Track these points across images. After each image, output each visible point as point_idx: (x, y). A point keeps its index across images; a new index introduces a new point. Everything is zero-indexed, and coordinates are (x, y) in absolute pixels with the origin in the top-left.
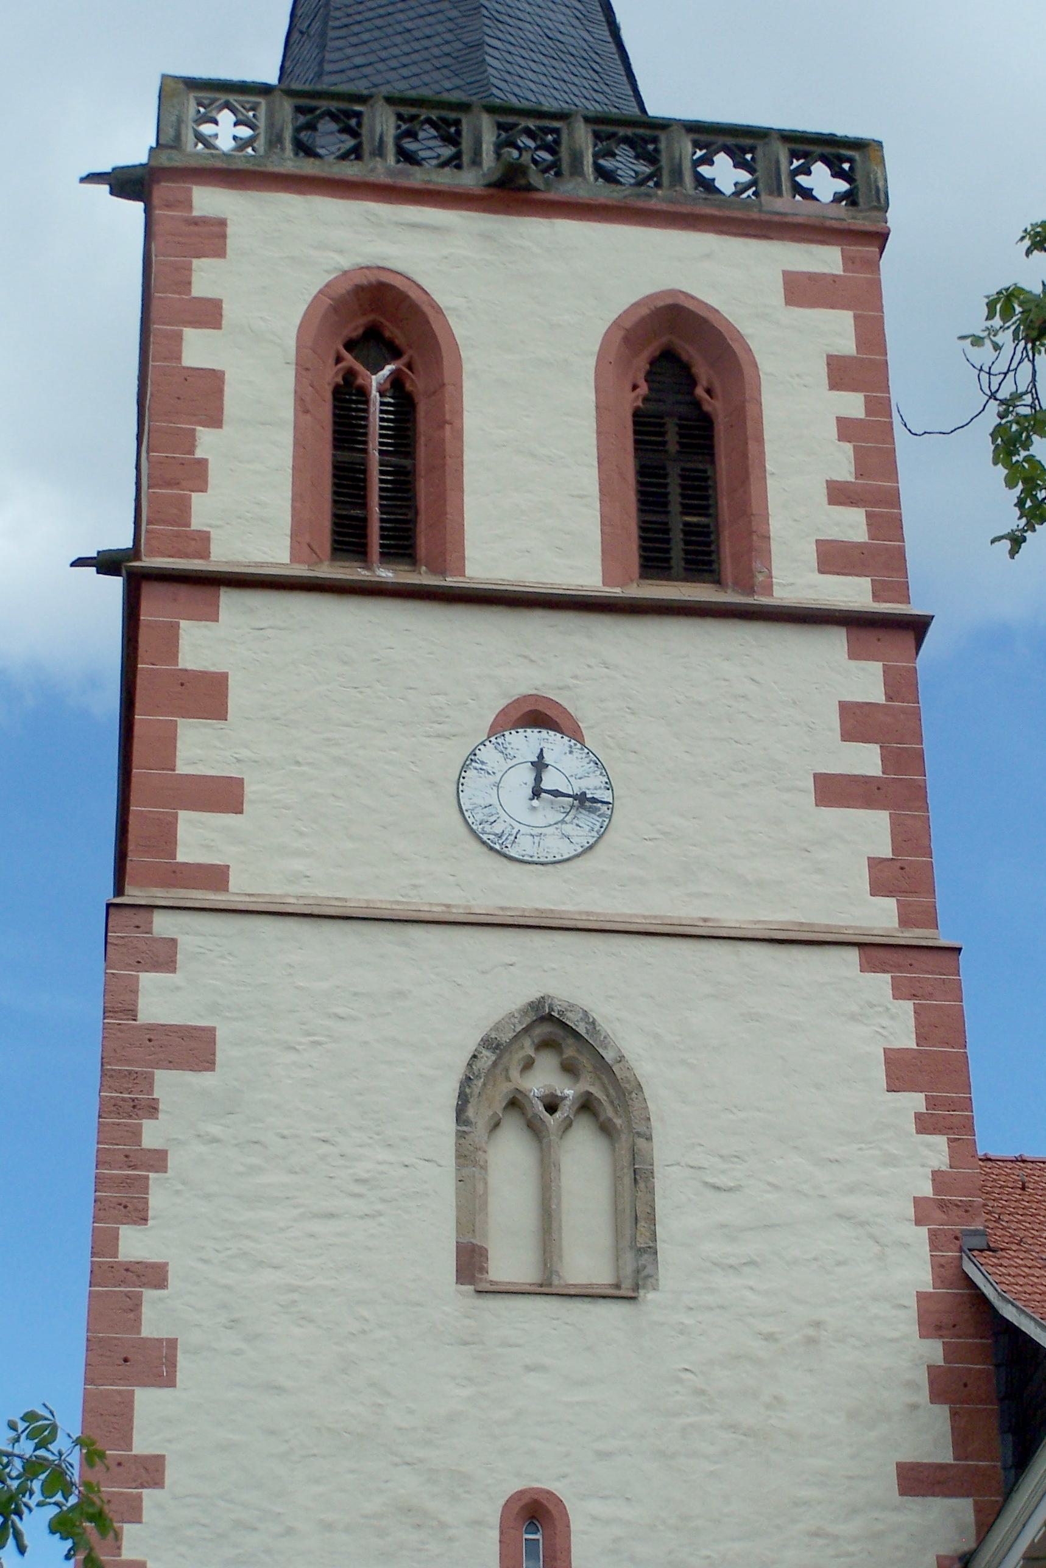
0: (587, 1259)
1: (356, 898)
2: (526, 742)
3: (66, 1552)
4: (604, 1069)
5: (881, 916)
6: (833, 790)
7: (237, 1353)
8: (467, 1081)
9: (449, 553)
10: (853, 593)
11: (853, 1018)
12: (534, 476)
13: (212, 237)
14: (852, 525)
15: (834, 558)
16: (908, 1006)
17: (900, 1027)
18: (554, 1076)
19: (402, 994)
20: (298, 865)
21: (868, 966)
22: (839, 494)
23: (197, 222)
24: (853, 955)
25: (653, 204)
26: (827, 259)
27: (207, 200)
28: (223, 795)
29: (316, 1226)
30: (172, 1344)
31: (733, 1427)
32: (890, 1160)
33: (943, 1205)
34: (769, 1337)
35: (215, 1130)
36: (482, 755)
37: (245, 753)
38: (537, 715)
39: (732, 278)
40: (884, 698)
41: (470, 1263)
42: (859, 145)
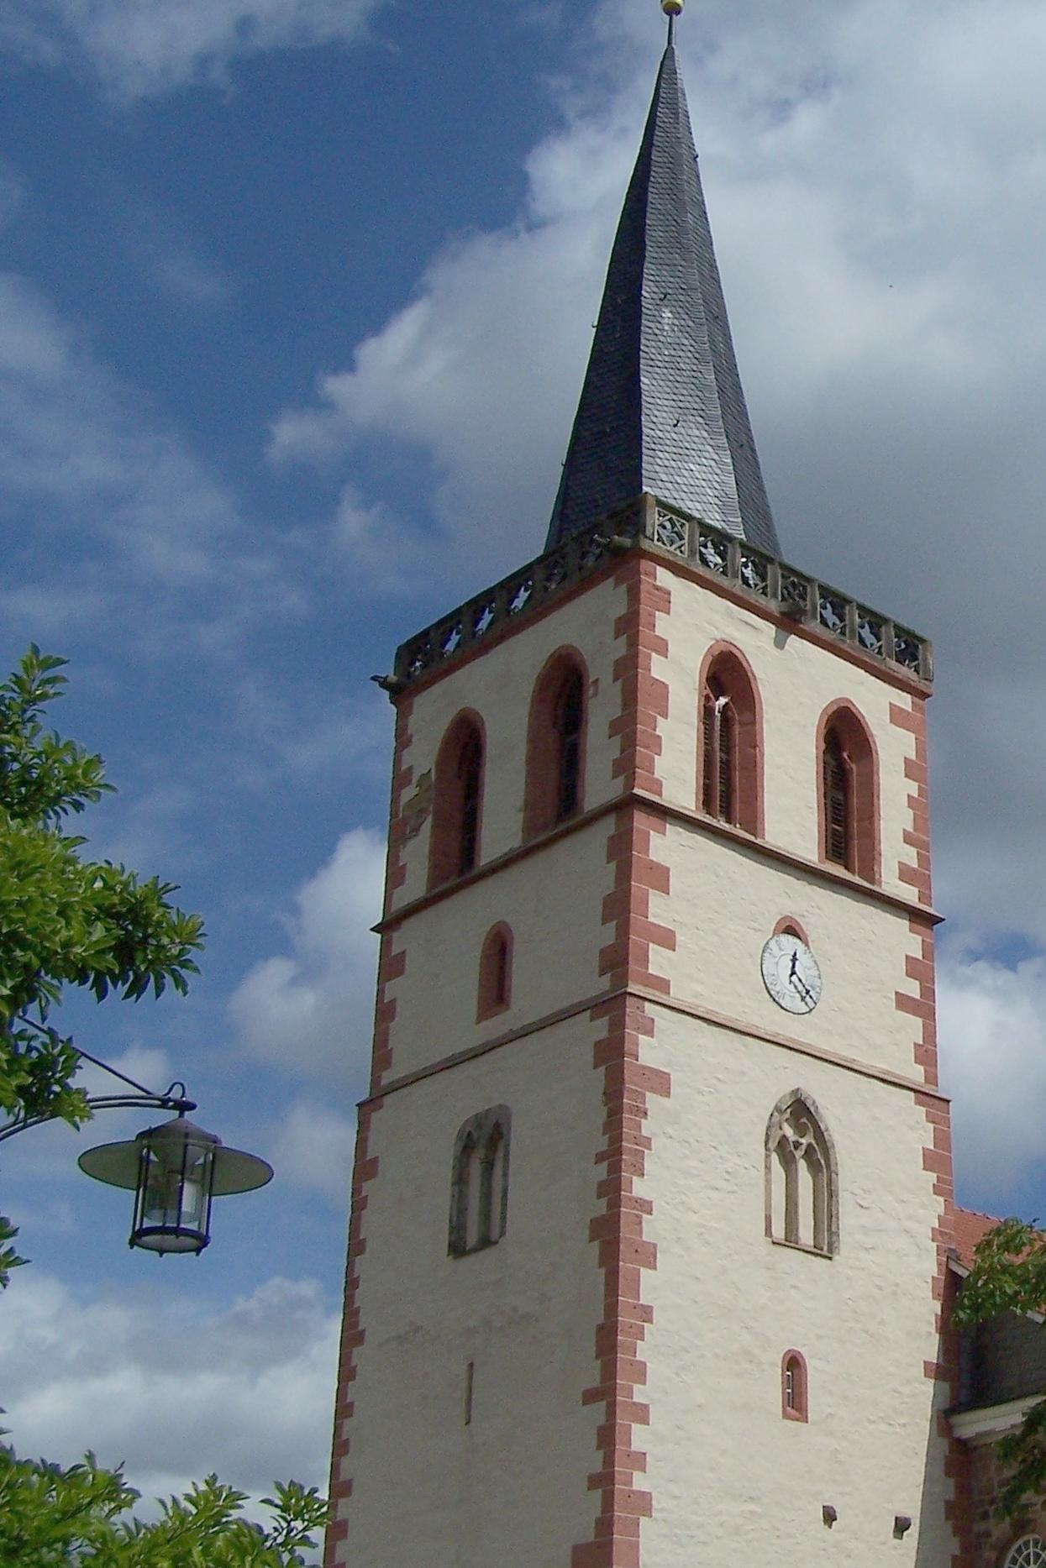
0: (806, 1235)
1: (725, 1014)
2: (789, 941)
3: (980, 1238)
4: (819, 1135)
5: (916, 1074)
6: (903, 1002)
7: (680, 1256)
8: (768, 1128)
9: (753, 822)
10: (908, 894)
11: (912, 1128)
12: (791, 809)
13: (664, 600)
14: (910, 856)
15: (906, 874)
16: (932, 1126)
17: (924, 1137)
18: (801, 1135)
19: (743, 1073)
20: (699, 988)
21: (918, 1103)
22: (908, 839)
23: (657, 588)
24: (912, 1094)
25: (844, 647)
26: (904, 701)
27: (664, 577)
28: (667, 939)
29: (711, 1193)
30: (655, 1246)
31: (866, 1332)
32: (923, 1206)
33: (941, 1233)
34: (880, 1288)
35: (670, 1131)
36: (772, 944)
37: (677, 917)
38: (791, 929)
39: (874, 700)
40: (651, 898)
41: (768, 1231)
42: (923, 641)
